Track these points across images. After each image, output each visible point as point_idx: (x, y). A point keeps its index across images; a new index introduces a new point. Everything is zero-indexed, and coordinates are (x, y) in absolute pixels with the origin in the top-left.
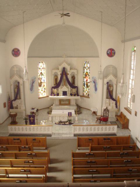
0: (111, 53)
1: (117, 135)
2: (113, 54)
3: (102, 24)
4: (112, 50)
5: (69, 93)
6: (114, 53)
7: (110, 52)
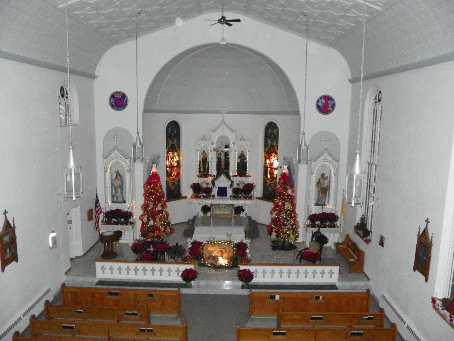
0: (326, 105)
1: (136, 163)
2: (330, 108)
3: (307, 40)
4: (327, 98)
5: (230, 192)
6: (333, 106)
7: (323, 103)
